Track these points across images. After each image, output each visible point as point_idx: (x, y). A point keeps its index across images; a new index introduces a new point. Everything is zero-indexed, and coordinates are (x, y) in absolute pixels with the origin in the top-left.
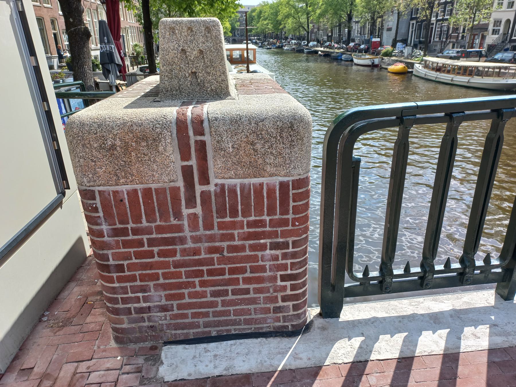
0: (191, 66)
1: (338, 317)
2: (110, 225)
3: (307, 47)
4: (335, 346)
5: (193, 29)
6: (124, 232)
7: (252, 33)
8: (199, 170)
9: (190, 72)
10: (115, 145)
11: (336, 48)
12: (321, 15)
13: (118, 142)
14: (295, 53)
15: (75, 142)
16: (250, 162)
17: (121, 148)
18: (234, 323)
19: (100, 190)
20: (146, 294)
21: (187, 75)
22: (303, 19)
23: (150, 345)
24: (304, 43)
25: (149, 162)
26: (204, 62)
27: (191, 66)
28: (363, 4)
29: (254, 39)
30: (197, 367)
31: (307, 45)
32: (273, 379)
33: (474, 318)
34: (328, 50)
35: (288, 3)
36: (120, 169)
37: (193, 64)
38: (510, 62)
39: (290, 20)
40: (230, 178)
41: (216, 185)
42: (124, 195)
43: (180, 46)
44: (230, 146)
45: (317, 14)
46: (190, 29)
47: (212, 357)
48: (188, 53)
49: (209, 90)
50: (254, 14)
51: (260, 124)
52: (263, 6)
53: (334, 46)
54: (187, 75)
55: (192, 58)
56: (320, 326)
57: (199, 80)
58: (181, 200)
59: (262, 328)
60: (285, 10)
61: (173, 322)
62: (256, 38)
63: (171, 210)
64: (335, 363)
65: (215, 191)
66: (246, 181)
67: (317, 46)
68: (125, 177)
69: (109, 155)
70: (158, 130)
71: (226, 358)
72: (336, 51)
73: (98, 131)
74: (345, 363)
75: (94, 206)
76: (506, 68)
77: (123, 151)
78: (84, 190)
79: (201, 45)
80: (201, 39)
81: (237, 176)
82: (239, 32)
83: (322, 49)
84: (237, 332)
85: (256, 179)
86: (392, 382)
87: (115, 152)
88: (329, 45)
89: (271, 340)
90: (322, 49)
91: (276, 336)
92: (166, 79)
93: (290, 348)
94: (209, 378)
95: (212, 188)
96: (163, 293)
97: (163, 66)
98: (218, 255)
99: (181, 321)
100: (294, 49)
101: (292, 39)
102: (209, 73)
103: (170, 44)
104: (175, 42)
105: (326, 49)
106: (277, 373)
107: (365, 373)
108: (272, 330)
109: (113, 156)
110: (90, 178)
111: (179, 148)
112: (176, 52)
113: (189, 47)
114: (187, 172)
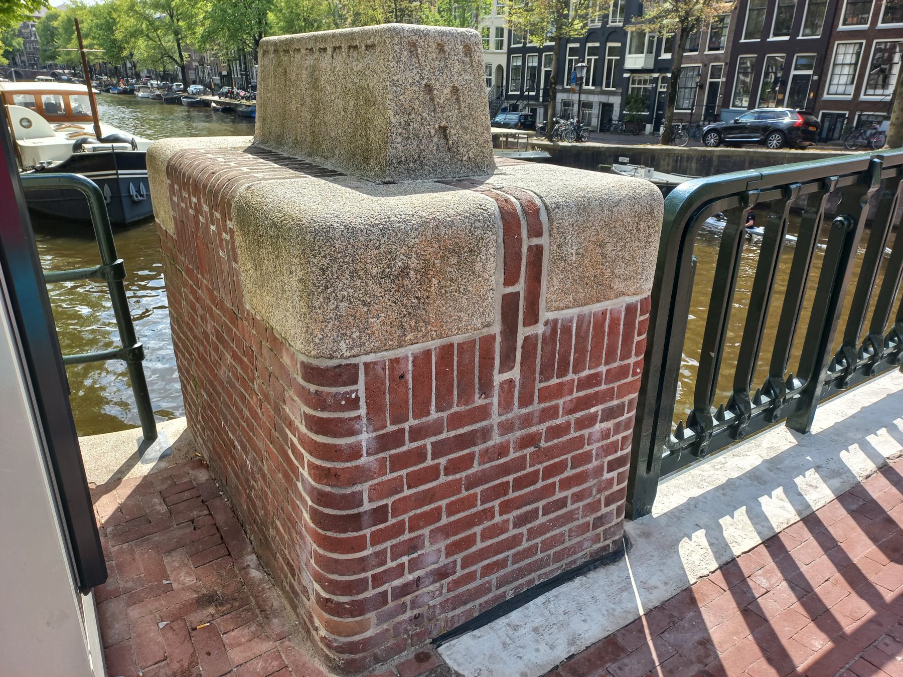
0: (440, 115)
1: (649, 512)
2: (375, 430)
3: (186, 94)
4: (681, 553)
5: (446, 48)
6: (396, 439)
7: (56, 62)
8: (527, 299)
9: (437, 126)
10: (408, 267)
11: (243, 98)
12: (208, 37)
13: (413, 263)
14: (162, 103)
15: (336, 267)
16: (595, 277)
17: (417, 272)
18: (542, 564)
19: (369, 361)
20: (415, 555)
21: (433, 131)
22: (169, 42)
23: (411, 656)
24: (177, 86)
25: (457, 294)
26: (459, 109)
27: (440, 115)
28: (282, 23)
29: (64, 74)
30: (525, 658)
31: (185, 90)
32: (647, 631)
33: (793, 464)
34: (228, 100)
35: (131, 8)
36: (410, 314)
37: (442, 112)
38: (515, 127)
39: (141, 43)
40: (567, 307)
41: (546, 323)
42: (407, 365)
43: (423, 79)
44: (574, 252)
45: (198, 35)
46: (441, 48)
47: (533, 633)
48: (435, 92)
49: (465, 158)
50: (55, 24)
51: (615, 209)
52: (73, 10)
53: (238, 94)
54: (433, 131)
55: (442, 101)
56: (638, 532)
57: (450, 142)
58: (493, 359)
59: (574, 561)
60: (127, 22)
61: (452, 594)
62: (66, 71)
63: (477, 380)
64: (701, 577)
65: (544, 334)
66: (586, 310)
67: (205, 93)
68: (417, 329)
69: (396, 288)
70: (479, 231)
71: (555, 627)
72: (244, 102)
73: (382, 241)
74: (713, 572)
75: (353, 396)
76: (514, 136)
77: (419, 277)
78: (335, 367)
79: (456, 78)
80: (457, 67)
81: (577, 303)
82: (25, 58)
83: (216, 98)
84: (542, 580)
85: (598, 305)
86: (784, 576)
87: (406, 282)
88: (229, 92)
89: (592, 575)
90: (216, 98)
91: (595, 568)
92: (399, 139)
93: (628, 577)
94: (557, 667)
95: (540, 329)
96: (442, 545)
97: (394, 116)
98: (532, 449)
99: (469, 587)
100: (158, 96)
101: (150, 78)
102: (466, 129)
103: (408, 74)
104: (415, 71)
105: (223, 99)
106: (644, 619)
107: (746, 576)
108: (588, 559)
109: (402, 289)
110: (353, 340)
111: (505, 263)
112: (417, 89)
113: (438, 80)
114: (509, 304)
